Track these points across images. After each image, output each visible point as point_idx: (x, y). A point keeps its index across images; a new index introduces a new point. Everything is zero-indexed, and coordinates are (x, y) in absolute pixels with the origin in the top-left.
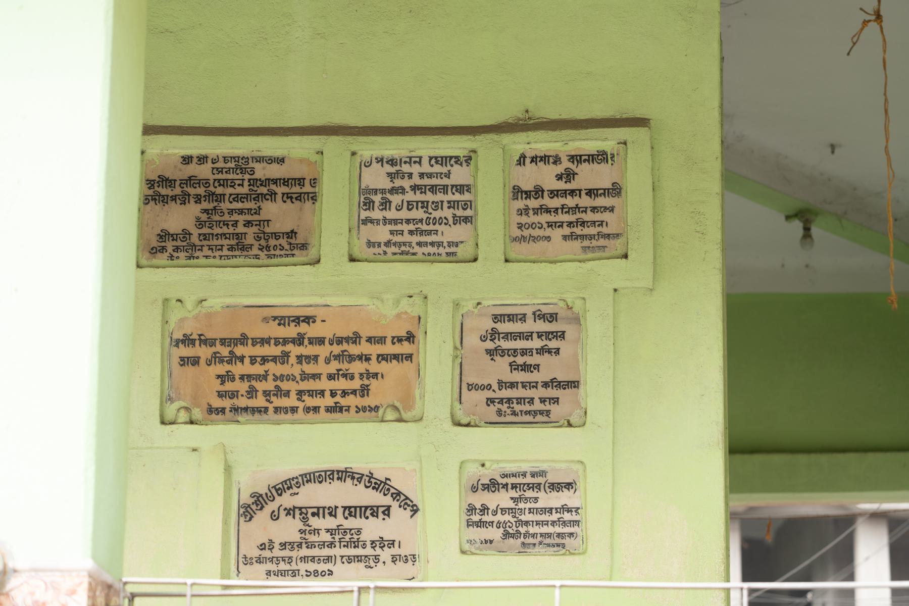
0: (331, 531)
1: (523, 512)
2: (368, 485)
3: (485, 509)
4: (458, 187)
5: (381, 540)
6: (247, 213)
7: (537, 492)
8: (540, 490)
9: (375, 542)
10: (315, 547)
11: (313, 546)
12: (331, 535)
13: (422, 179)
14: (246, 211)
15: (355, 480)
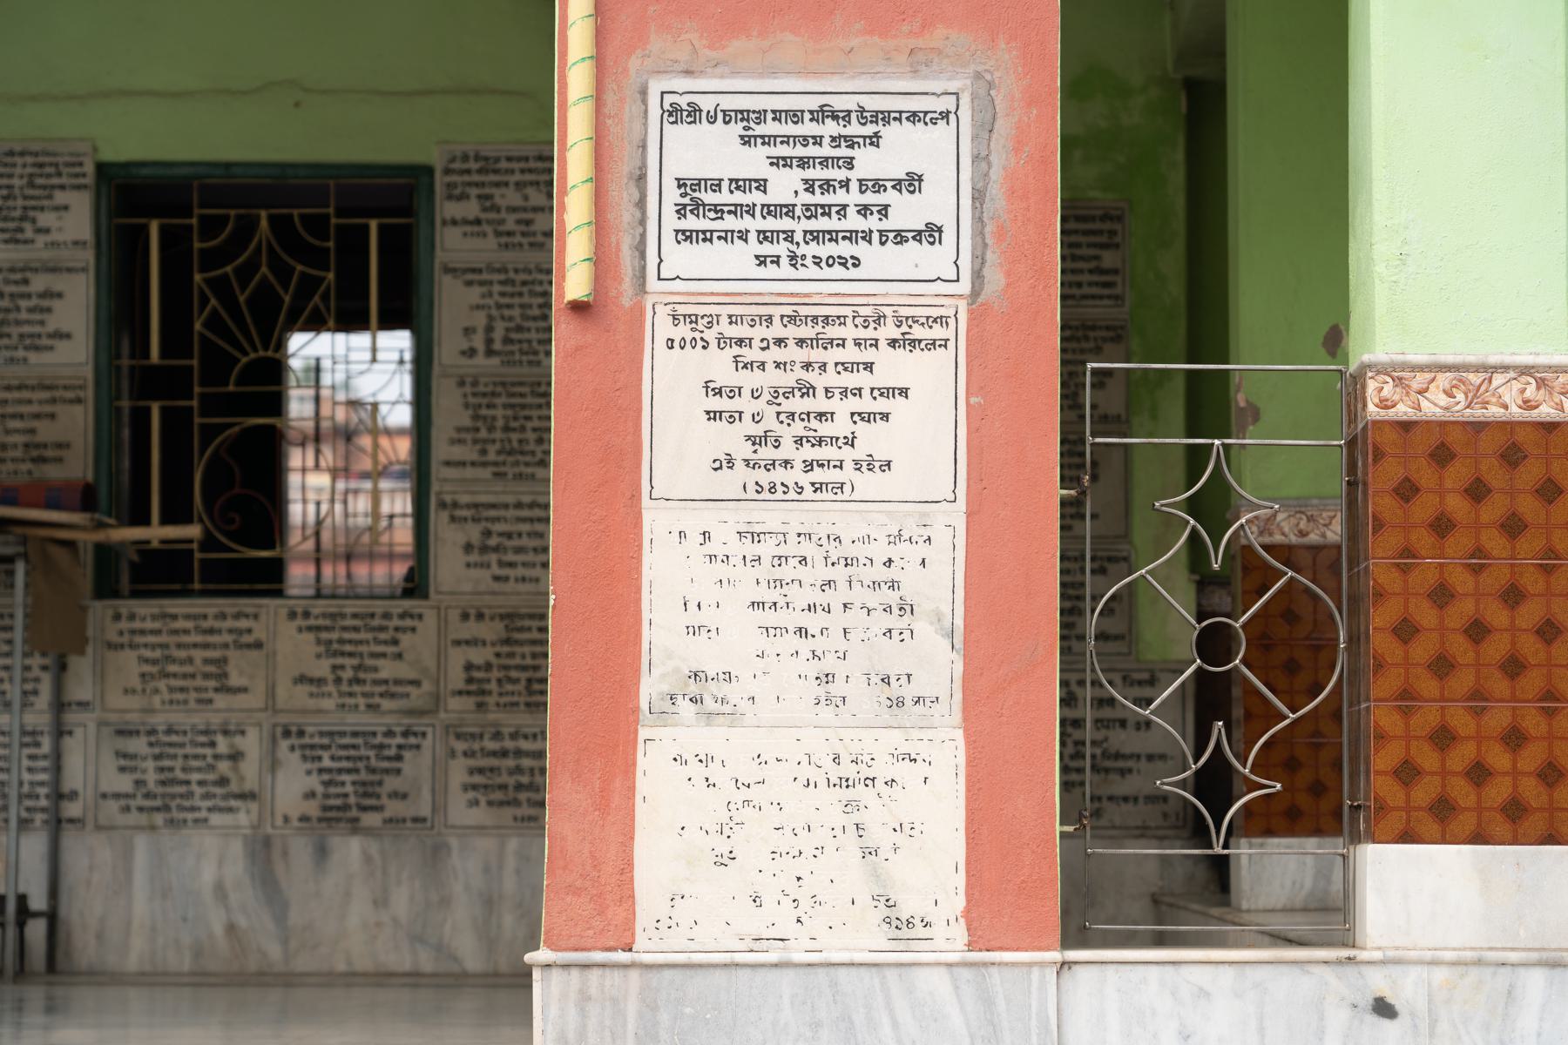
0: (753, 439)
1: (762, 117)
2: (863, 121)
3: (695, 111)
4: (772, 208)
6: (862, 143)
7: (845, 126)
8: (849, 122)
12: (754, 444)
14: (861, 141)
15: (840, 121)
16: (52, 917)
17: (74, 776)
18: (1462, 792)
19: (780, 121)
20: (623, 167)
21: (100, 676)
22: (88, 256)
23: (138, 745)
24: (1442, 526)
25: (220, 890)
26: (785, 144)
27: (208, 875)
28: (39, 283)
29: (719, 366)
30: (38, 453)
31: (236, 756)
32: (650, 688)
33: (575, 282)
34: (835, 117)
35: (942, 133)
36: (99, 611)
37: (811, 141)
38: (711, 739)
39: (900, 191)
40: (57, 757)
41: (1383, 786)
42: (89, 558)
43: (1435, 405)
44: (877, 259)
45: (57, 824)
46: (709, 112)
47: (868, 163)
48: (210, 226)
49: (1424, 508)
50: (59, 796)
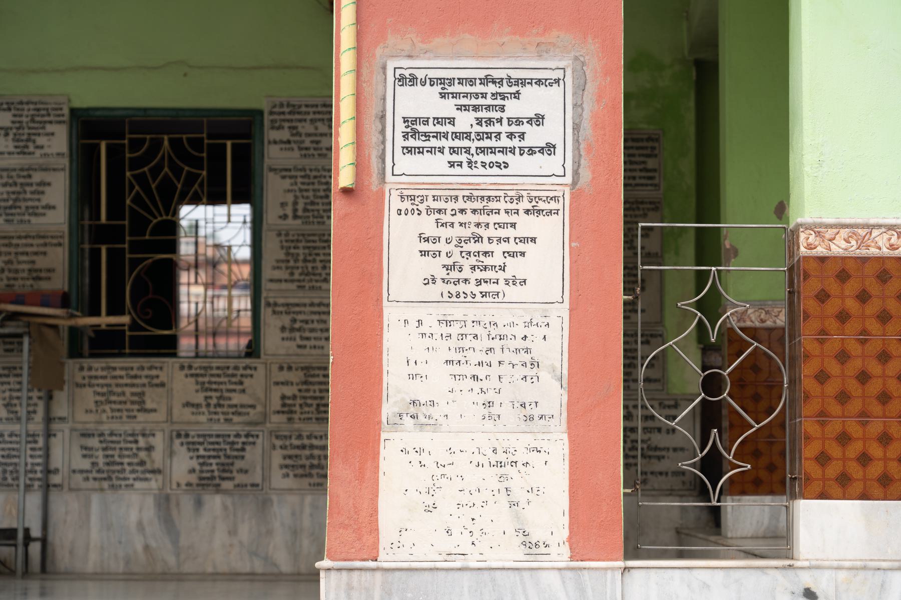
1: (452, 82)
5: (514, 278)
6: (509, 97)
9: (514, 134)
10: (450, 283)
11: (521, 123)
13: (524, 87)
14: (509, 95)
16: (44, 541)
17: (57, 460)
18: (855, 470)
19: (462, 84)
20: (372, 110)
21: (72, 402)
22: (65, 162)
23: (94, 442)
24: (843, 317)
25: (140, 526)
26: (429, 153)
27: (133, 517)
28: (37, 177)
29: (428, 225)
30: (36, 275)
31: (150, 449)
32: (387, 410)
33: (344, 177)
34: (494, 82)
35: (556, 90)
36: (71, 365)
37: (480, 96)
38: (423, 439)
39: (531, 124)
40: (47, 449)
41: (810, 467)
42: (65, 335)
43: (839, 247)
44: (518, 164)
45: (47, 488)
46: (421, 79)
47: (513, 108)
48: (135, 145)
49: (832, 307)
50: (48, 471)
